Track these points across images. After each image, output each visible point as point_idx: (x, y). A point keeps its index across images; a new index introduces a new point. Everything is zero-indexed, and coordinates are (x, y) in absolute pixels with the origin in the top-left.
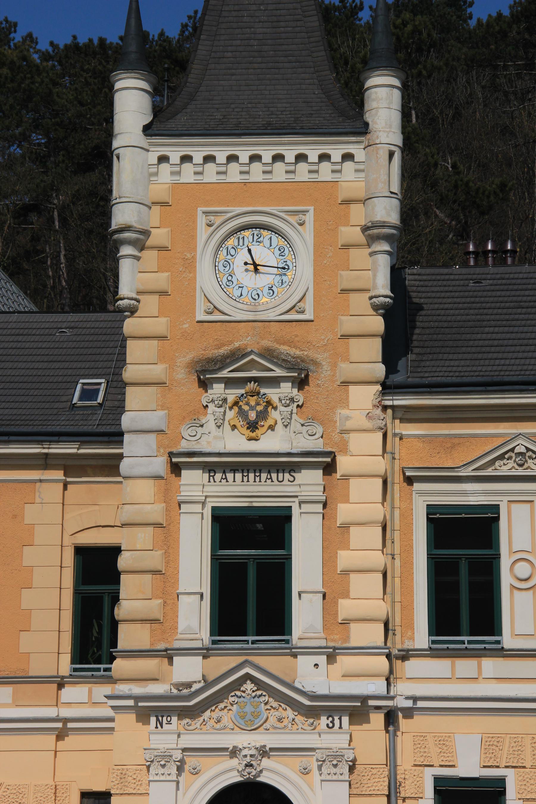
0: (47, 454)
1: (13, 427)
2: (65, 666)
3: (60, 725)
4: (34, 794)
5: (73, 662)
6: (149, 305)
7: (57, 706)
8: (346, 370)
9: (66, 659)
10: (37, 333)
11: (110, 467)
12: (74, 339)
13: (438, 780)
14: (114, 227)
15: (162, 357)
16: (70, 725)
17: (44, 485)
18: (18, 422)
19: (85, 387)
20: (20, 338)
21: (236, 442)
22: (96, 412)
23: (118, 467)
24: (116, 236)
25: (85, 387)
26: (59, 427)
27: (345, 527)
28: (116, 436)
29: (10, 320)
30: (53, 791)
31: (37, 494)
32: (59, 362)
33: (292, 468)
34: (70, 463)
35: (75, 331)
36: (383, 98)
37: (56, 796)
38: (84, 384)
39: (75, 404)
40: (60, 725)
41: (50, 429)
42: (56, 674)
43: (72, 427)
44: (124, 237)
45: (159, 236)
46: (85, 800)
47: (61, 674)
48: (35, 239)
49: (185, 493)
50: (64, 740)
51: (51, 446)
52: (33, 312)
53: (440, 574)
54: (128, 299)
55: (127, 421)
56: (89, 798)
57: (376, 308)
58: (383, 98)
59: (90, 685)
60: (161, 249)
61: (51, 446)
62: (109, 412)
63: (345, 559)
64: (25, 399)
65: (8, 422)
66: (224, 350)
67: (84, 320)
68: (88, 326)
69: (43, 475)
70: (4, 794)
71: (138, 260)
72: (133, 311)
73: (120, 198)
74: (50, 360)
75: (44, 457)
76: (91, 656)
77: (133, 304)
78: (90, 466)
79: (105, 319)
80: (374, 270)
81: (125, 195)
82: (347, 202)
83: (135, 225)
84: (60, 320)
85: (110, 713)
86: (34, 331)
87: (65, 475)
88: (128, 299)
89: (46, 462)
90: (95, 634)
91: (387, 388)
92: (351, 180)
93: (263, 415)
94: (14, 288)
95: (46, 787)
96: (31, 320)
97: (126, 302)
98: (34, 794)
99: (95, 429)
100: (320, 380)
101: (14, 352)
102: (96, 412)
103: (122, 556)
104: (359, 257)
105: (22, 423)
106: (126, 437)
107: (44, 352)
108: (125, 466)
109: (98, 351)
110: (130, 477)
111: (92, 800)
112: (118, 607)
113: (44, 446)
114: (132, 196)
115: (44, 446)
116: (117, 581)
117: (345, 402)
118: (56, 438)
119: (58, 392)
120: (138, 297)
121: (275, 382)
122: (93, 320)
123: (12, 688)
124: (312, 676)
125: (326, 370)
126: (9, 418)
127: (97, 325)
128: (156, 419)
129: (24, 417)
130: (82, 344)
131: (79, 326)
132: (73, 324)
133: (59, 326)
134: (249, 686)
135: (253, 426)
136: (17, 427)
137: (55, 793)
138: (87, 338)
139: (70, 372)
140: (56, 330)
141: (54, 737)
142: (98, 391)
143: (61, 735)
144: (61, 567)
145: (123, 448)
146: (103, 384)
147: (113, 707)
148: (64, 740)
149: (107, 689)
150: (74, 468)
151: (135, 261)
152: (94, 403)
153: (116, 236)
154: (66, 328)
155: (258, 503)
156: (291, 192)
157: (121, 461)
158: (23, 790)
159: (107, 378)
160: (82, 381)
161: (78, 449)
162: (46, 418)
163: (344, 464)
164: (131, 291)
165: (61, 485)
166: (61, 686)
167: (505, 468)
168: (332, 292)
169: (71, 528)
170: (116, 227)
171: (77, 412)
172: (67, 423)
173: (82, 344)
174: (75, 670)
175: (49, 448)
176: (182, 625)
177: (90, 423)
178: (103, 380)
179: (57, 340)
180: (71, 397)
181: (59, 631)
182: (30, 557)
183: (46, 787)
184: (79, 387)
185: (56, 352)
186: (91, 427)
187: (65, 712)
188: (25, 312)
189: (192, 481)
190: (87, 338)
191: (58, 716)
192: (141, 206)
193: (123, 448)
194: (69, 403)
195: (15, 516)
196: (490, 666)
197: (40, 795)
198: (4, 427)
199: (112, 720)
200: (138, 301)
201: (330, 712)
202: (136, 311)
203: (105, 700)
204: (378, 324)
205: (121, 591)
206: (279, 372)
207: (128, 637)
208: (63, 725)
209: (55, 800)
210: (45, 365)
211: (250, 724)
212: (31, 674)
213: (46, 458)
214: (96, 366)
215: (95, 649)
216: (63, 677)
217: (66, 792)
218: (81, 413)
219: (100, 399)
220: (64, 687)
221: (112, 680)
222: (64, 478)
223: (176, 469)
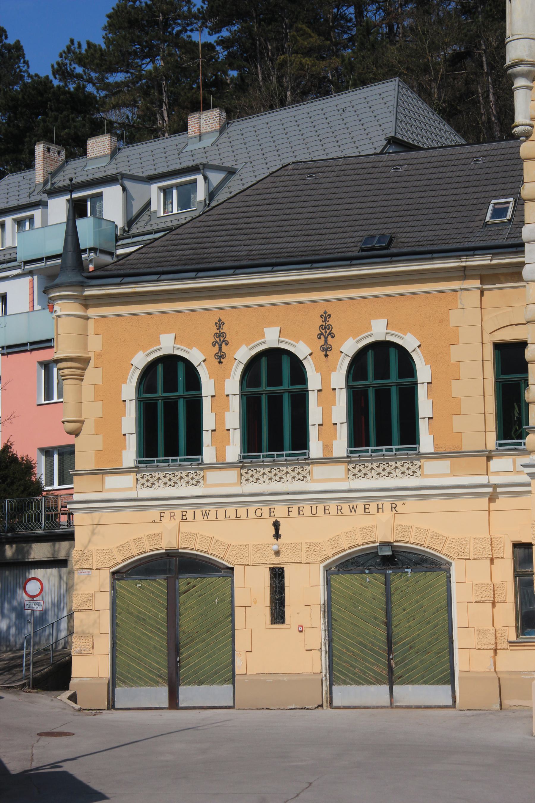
0: (465, 267)
1: (435, 246)
2: (492, 442)
3: (490, 490)
4: (474, 545)
5: (498, 438)
7: (487, 474)
9: (492, 436)
10: (456, 164)
11: (515, 273)
12: (487, 166)
14: (508, 62)
16: (499, 490)
17: (465, 293)
18: (440, 242)
19: (496, 206)
20: (441, 170)
22: (505, 227)
23: (520, 274)
24: (510, 70)
25: (496, 206)
26: (474, 243)
28: (518, 247)
29: (433, 155)
30: (490, 543)
31: (459, 301)
32: (466, 187)
34: (484, 272)
35: (488, 158)
37: (492, 547)
38: (495, 204)
39: (488, 222)
40: (490, 490)
41: (466, 245)
42: (484, 449)
43: (485, 242)
44: (518, 70)
46: (517, 550)
47: (488, 448)
48: (467, 83)
50: (495, 502)
51: (468, 260)
52: (462, 145)
54: (523, 125)
55: (526, 232)
56: (520, 548)
59: (514, 457)
61: (468, 260)
62: (517, 226)
64: (446, 221)
65: (432, 242)
67: (495, 148)
68: (499, 153)
69: (463, 284)
70: (450, 546)
71: (531, 90)
72: (527, 136)
73: (512, 36)
74: (466, 186)
75: (463, 269)
76: (514, 433)
77: (528, 130)
78: (503, 274)
79: (514, 146)
81: (517, 33)
83: (526, 58)
84: (474, 151)
85: (525, 479)
86: (453, 163)
87: (481, 283)
88: (523, 125)
89: (464, 273)
90: (517, 415)
94: (447, 127)
95: (484, 540)
96: (450, 153)
97: (521, 128)
98: (474, 545)
99: (505, 242)
101: (436, 182)
102: (505, 227)
103: (529, 349)
105: (443, 242)
106: (527, 247)
107: (461, 179)
108: (526, 272)
109: (508, 174)
110: (532, 281)
111: (522, 550)
112: (527, 391)
113: (462, 260)
114: (523, 33)
115: (462, 260)
116: (525, 370)
118: (471, 253)
119: (474, 213)
120: (531, 123)
122: (503, 147)
123: (344, 466)
126: (433, 239)
127: (507, 151)
129: (452, 236)
130: (493, 170)
131: (491, 154)
132: (485, 153)
133: (474, 156)
136: (439, 246)
137: (491, 544)
138: (498, 164)
139: (483, 195)
140: (471, 159)
141: (487, 499)
142: (507, 209)
143: (492, 498)
144: (483, 361)
145: (524, 257)
146: (511, 203)
147: (529, 474)
148: (495, 502)
149: (526, 460)
150: (488, 276)
151: (528, 90)
152: (504, 220)
153: (510, 71)
154: (480, 157)
157: (523, 268)
158: (465, 542)
159: (515, 197)
160: (493, 201)
161: (491, 260)
162: (463, 236)
164: (525, 118)
165: (479, 292)
166: (489, 458)
169: (489, 327)
170: (510, 63)
171: (489, 229)
172: (481, 238)
173: (493, 170)
174: (500, 445)
175: (466, 261)
177: (500, 237)
178: (511, 199)
179: (472, 168)
180: (484, 216)
181: (485, 414)
182: (456, 353)
183: (484, 540)
184: (491, 206)
185: (472, 178)
186: (501, 240)
187: (495, 480)
188: (456, 146)
190: (498, 164)
191: (489, 482)
192: (532, 40)
193: (524, 257)
194: (483, 222)
195: (441, 321)
197: (479, 546)
198: (428, 246)
199: (529, 485)
200: (532, 126)
202: (531, 135)
203: (522, 468)
205: (529, 378)
208: (493, 490)
209: (492, 550)
210: (463, 190)
212: (463, 450)
213: (465, 270)
214: (505, 188)
215: (517, 427)
216: (490, 451)
217: (500, 544)
218: (493, 229)
219: (509, 216)
220: (492, 459)
221: (526, 452)
222: (481, 286)
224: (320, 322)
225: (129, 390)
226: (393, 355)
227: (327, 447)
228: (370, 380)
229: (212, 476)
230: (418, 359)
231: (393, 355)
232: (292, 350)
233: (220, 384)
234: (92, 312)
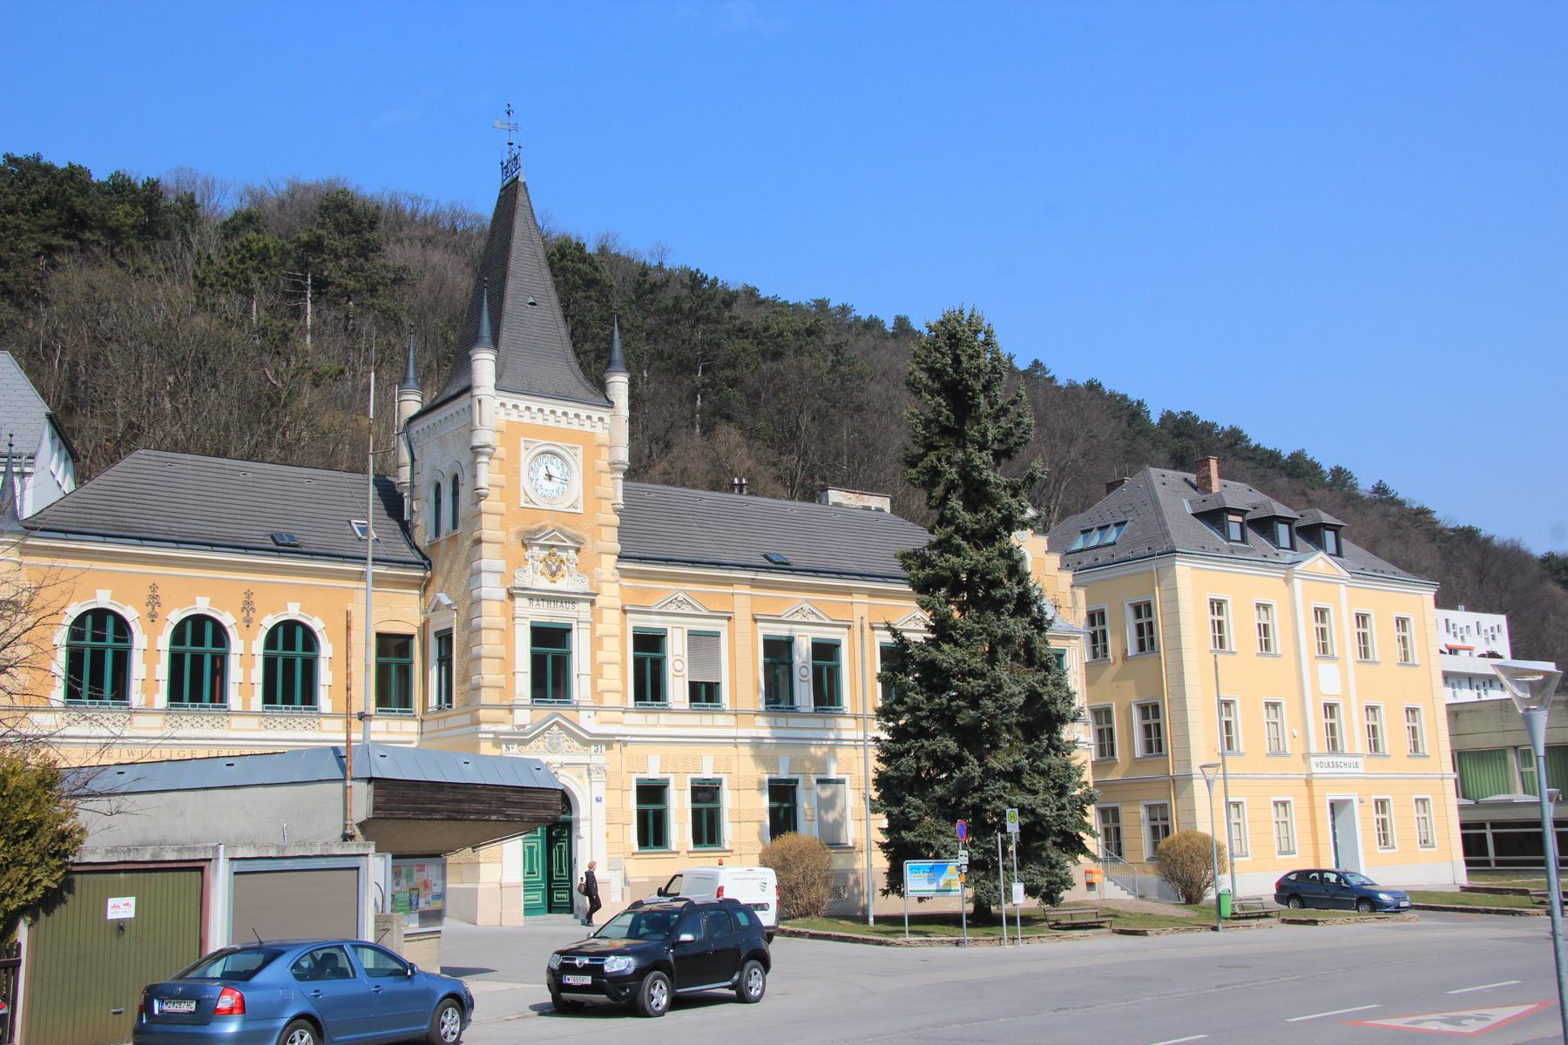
6: (494, 494)
8: (601, 545)
9: (373, 703)
13: (693, 781)
15: (502, 528)
21: (543, 583)
27: (600, 638)
33: (574, 601)
36: (619, 385)
45: (501, 451)
49: (518, 612)
53: (538, 663)
57: (615, 511)
58: (619, 385)
60: (501, 460)
63: (601, 656)
66: (535, 527)
80: (615, 488)
82: (600, 446)
91: (621, 557)
92: (601, 433)
93: (559, 568)
100: (587, 549)
104: (606, 478)
117: (599, 564)
121: (565, 549)
124: (589, 722)
125: (589, 545)
128: (500, 564)
134: (555, 728)
135: (553, 574)
155: (555, 620)
156: (569, 436)
163: (600, 600)
167: (672, 609)
168: (593, 499)
169: (374, 620)
176: (518, 692)
189: (521, 603)
196: (664, 718)
201: (597, 743)
204: (616, 520)
206: (569, 543)
207: (487, 696)
211: (553, 749)
223: (511, 596)
224: (244, 598)
225: (61, 637)
226: (110, 622)
227: (246, 702)
228: (188, 646)
229: (236, 721)
230: (233, 634)
231: (110, 622)
232: (308, 623)
233: (152, 640)
234: (27, 560)
